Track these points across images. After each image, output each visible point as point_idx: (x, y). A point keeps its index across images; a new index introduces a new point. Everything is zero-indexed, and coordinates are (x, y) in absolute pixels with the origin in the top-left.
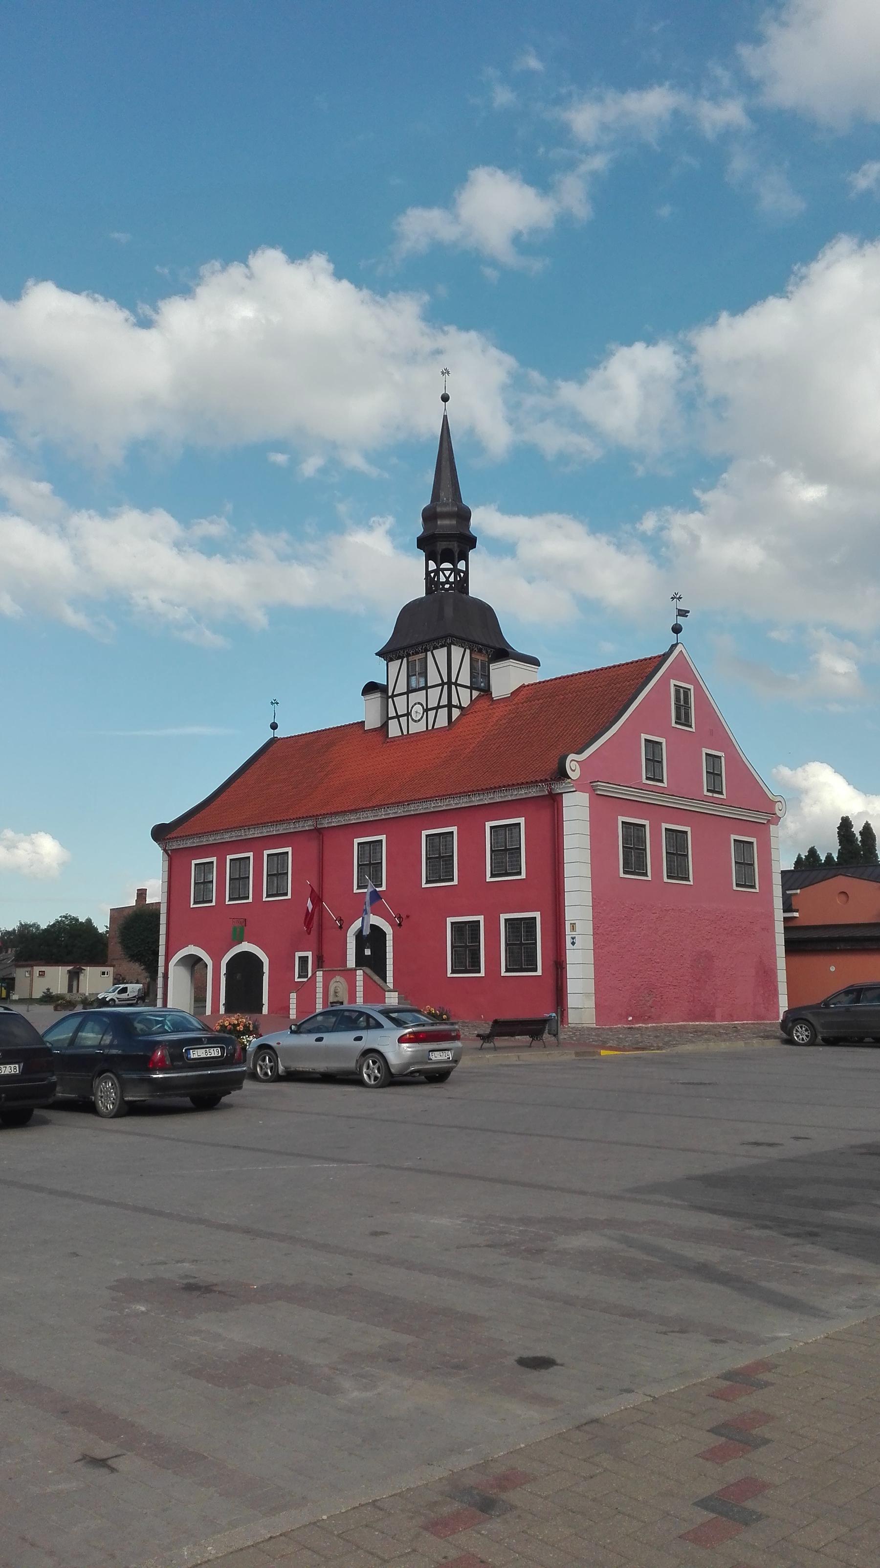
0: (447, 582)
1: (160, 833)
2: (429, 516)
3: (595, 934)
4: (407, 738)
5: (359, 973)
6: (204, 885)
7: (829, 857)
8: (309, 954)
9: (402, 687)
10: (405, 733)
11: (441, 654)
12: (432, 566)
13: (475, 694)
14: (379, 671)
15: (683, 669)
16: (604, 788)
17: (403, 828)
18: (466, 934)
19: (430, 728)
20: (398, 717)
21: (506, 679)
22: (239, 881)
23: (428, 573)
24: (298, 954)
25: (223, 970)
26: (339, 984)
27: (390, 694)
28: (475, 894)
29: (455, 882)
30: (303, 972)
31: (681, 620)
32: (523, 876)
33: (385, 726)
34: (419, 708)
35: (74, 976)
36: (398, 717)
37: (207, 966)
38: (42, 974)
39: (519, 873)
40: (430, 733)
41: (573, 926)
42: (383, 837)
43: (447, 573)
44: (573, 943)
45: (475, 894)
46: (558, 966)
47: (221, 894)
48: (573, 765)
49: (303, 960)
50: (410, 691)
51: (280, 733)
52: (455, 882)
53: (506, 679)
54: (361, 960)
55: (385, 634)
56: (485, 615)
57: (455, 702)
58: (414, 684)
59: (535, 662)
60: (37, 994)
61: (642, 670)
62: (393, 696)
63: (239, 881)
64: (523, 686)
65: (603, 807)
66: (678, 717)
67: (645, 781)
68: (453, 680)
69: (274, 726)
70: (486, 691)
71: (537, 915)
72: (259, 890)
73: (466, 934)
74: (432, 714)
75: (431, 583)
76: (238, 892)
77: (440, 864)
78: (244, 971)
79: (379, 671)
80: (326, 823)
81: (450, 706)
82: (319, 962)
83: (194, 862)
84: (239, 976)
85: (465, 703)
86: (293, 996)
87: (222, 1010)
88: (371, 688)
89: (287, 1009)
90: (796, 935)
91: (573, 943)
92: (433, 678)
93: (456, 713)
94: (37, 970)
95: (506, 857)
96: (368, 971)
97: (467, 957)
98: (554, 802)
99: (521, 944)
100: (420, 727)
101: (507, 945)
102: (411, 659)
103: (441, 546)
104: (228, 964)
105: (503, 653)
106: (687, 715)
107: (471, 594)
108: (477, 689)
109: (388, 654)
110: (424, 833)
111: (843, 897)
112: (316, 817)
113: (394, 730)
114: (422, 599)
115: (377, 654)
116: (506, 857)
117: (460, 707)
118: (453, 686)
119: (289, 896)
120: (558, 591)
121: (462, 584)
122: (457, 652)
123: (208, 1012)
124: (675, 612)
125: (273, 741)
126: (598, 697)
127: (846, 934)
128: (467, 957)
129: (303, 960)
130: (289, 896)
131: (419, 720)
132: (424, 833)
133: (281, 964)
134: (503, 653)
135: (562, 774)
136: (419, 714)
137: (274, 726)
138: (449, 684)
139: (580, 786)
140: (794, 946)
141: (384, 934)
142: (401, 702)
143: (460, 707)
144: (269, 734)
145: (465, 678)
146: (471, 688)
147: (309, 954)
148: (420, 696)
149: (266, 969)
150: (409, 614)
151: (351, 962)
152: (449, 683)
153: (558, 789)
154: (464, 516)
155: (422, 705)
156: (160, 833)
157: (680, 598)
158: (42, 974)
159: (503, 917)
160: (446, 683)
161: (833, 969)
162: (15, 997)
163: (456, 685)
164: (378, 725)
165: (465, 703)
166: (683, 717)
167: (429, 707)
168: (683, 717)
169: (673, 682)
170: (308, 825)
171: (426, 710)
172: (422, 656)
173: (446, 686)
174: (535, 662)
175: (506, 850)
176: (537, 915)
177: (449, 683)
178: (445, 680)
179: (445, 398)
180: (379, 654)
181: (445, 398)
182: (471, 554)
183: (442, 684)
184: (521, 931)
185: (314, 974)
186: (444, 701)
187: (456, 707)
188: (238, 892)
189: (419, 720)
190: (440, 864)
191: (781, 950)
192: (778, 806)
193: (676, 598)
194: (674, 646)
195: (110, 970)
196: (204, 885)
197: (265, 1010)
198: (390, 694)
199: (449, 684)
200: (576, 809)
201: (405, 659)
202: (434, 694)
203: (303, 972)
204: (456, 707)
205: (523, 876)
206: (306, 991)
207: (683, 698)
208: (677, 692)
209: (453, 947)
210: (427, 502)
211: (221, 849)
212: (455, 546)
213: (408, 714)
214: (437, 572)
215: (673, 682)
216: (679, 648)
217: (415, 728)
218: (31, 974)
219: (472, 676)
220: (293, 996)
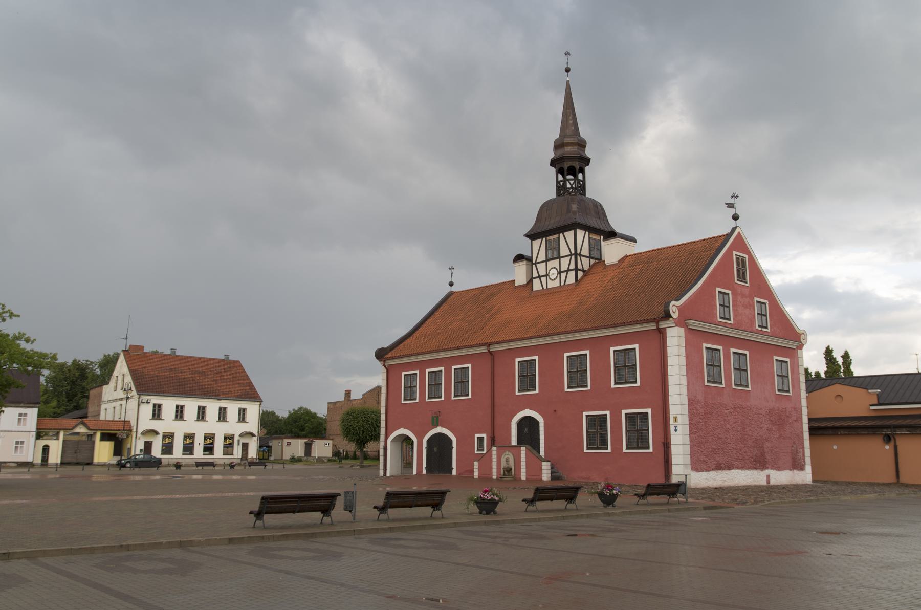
0: (572, 188)
1: (381, 354)
2: (558, 145)
3: (690, 424)
4: (547, 293)
5: (523, 448)
6: (410, 389)
7: (817, 374)
8: (484, 435)
9: (542, 257)
11: (569, 235)
12: (560, 177)
13: (592, 261)
14: (525, 246)
15: (741, 244)
16: (693, 324)
17: (551, 352)
18: (597, 423)
20: (539, 277)
21: (612, 252)
22: (435, 386)
23: (558, 182)
24: (477, 435)
25: (425, 445)
26: (508, 456)
28: (602, 395)
29: (589, 388)
30: (481, 447)
31: (732, 211)
32: (638, 384)
33: (530, 282)
34: (554, 271)
35: (308, 447)
36: (539, 277)
38: (289, 444)
39: (636, 382)
40: (562, 288)
41: (675, 418)
42: (536, 358)
43: (572, 182)
44: (676, 430)
45: (602, 395)
46: (666, 446)
47: (423, 395)
48: (674, 307)
49: (481, 440)
50: (547, 260)
51: (455, 289)
52: (589, 388)
53: (612, 252)
54: (520, 441)
56: (598, 210)
57: (579, 267)
58: (549, 256)
59: (633, 240)
60: (287, 456)
61: (714, 245)
62: (536, 263)
63: (435, 386)
64: (627, 256)
65: (694, 337)
66: (739, 276)
67: (719, 320)
69: (451, 284)
70: (600, 260)
71: (649, 411)
72: (448, 392)
73: (597, 423)
74: (563, 275)
75: (561, 189)
76: (435, 393)
77: (577, 376)
78: (439, 446)
79: (525, 246)
80: (494, 348)
81: (576, 269)
82: (493, 441)
83: (404, 373)
84: (435, 449)
85: (586, 268)
86: (476, 463)
87: (424, 472)
88: (519, 258)
89: (472, 471)
90: (816, 425)
91: (676, 430)
92: (564, 251)
93: (580, 274)
94: (286, 441)
95: (625, 370)
96: (529, 447)
97: (598, 438)
98: (662, 332)
99: (638, 430)
100: (556, 284)
101: (627, 431)
102: (548, 238)
103: (566, 165)
104: (428, 441)
105: (611, 235)
106: (744, 274)
107: (587, 195)
108: (593, 258)
109: (532, 236)
110: (566, 355)
111: (839, 399)
112: (489, 345)
113: (537, 285)
114: (554, 199)
116: (625, 370)
117: (583, 271)
119: (470, 397)
121: (581, 188)
122: (580, 233)
123: (415, 472)
124: (736, 206)
125: (451, 294)
126: (686, 265)
127: (846, 424)
128: (598, 438)
129: (481, 440)
130: (470, 397)
132: (566, 355)
133: (464, 441)
134: (611, 235)
135: (667, 316)
136: (554, 275)
137: (451, 284)
138: (576, 255)
139: (680, 323)
140: (812, 430)
141: (538, 423)
142: (542, 268)
143: (583, 271)
145: (585, 251)
146: (590, 257)
147: (484, 435)
148: (555, 263)
149: (454, 444)
150: (546, 208)
151: (514, 442)
152: (576, 254)
153: (663, 325)
154: (582, 144)
156: (381, 354)
158: (289, 444)
159: (624, 412)
162: (272, 458)
163: (580, 255)
164: (525, 282)
165: (586, 268)
166: (742, 276)
168: (742, 276)
169: (735, 253)
170: (484, 349)
171: (560, 272)
172: (557, 236)
174: (633, 240)
175: (625, 366)
176: (649, 411)
177: (576, 254)
178: (573, 252)
179: (568, 70)
180: (526, 236)
181: (568, 70)
182: (587, 169)
183: (571, 255)
184: (637, 424)
185: (489, 450)
186: (572, 266)
188: (435, 393)
190: (577, 376)
191: (806, 435)
192: (802, 337)
193: (734, 196)
194: (734, 229)
195: (331, 442)
196: (410, 389)
197: (454, 472)
199: (576, 255)
200: (675, 338)
202: (565, 263)
203: (481, 447)
205: (638, 384)
206: (485, 460)
207: (741, 262)
208: (738, 259)
209: (587, 432)
210: (557, 135)
211: (422, 365)
212: (577, 165)
213: (547, 275)
214: (565, 180)
215: (735, 253)
216: (738, 230)
217: (551, 284)
218: (282, 444)
219: (590, 250)
220: (476, 463)
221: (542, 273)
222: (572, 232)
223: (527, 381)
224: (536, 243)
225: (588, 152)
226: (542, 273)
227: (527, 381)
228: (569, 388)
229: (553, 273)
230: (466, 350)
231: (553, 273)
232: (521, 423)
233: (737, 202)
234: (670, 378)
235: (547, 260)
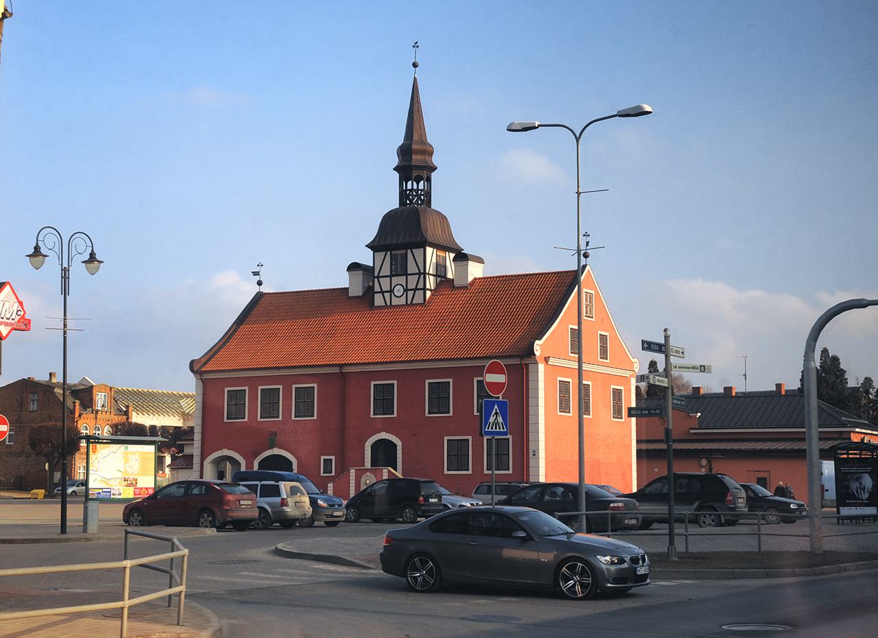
10: (388, 304)
13: (439, 279)
14: (367, 258)
19: (409, 303)
20: (382, 292)
27: (376, 275)
31: (257, 278)
36: (382, 292)
37: (240, 464)
49: (328, 462)
50: (391, 276)
51: (265, 289)
55: (371, 233)
57: (428, 287)
62: (378, 277)
68: (427, 272)
74: (410, 294)
75: (404, 195)
90: (823, 436)
92: (411, 268)
93: (428, 294)
100: (402, 301)
102: (393, 252)
107: (432, 207)
108: (439, 276)
112: (341, 366)
115: (366, 246)
118: (427, 276)
120: (496, 227)
124: (261, 273)
125: (260, 296)
129: (328, 462)
131: (400, 297)
137: (260, 283)
143: (431, 290)
144: (256, 289)
148: (402, 280)
155: (402, 286)
157: (262, 265)
160: (376, 277)
161: (656, 470)
163: (419, 274)
167: (409, 288)
170: (336, 370)
171: (406, 290)
172: (404, 251)
173: (422, 276)
178: (422, 271)
179: (416, 46)
187: (428, 290)
189: (400, 297)
198: (376, 275)
201: (389, 253)
204: (428, 290)
213: (391, 291)
217: (395, 302)
221: (386, 287)
222: (384, 253)
223: (384, 403)
224: (380, 255)
225: (435, 160)
226: (386, 287)
227: (384, 403)
228: (261, 418)
229: (399, 291)
230: (452, 362)
231: (399, 291)
232: (375, 446)
233: (262, 270)
234: (749, 390)
235: (391, 276)
